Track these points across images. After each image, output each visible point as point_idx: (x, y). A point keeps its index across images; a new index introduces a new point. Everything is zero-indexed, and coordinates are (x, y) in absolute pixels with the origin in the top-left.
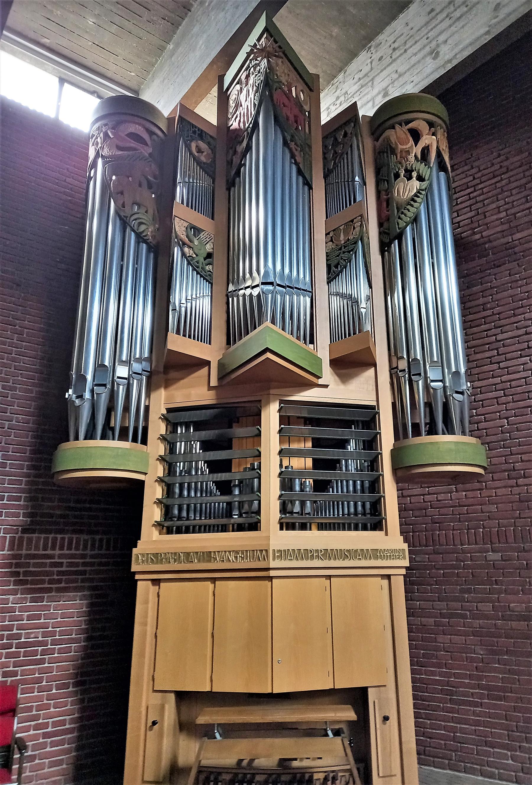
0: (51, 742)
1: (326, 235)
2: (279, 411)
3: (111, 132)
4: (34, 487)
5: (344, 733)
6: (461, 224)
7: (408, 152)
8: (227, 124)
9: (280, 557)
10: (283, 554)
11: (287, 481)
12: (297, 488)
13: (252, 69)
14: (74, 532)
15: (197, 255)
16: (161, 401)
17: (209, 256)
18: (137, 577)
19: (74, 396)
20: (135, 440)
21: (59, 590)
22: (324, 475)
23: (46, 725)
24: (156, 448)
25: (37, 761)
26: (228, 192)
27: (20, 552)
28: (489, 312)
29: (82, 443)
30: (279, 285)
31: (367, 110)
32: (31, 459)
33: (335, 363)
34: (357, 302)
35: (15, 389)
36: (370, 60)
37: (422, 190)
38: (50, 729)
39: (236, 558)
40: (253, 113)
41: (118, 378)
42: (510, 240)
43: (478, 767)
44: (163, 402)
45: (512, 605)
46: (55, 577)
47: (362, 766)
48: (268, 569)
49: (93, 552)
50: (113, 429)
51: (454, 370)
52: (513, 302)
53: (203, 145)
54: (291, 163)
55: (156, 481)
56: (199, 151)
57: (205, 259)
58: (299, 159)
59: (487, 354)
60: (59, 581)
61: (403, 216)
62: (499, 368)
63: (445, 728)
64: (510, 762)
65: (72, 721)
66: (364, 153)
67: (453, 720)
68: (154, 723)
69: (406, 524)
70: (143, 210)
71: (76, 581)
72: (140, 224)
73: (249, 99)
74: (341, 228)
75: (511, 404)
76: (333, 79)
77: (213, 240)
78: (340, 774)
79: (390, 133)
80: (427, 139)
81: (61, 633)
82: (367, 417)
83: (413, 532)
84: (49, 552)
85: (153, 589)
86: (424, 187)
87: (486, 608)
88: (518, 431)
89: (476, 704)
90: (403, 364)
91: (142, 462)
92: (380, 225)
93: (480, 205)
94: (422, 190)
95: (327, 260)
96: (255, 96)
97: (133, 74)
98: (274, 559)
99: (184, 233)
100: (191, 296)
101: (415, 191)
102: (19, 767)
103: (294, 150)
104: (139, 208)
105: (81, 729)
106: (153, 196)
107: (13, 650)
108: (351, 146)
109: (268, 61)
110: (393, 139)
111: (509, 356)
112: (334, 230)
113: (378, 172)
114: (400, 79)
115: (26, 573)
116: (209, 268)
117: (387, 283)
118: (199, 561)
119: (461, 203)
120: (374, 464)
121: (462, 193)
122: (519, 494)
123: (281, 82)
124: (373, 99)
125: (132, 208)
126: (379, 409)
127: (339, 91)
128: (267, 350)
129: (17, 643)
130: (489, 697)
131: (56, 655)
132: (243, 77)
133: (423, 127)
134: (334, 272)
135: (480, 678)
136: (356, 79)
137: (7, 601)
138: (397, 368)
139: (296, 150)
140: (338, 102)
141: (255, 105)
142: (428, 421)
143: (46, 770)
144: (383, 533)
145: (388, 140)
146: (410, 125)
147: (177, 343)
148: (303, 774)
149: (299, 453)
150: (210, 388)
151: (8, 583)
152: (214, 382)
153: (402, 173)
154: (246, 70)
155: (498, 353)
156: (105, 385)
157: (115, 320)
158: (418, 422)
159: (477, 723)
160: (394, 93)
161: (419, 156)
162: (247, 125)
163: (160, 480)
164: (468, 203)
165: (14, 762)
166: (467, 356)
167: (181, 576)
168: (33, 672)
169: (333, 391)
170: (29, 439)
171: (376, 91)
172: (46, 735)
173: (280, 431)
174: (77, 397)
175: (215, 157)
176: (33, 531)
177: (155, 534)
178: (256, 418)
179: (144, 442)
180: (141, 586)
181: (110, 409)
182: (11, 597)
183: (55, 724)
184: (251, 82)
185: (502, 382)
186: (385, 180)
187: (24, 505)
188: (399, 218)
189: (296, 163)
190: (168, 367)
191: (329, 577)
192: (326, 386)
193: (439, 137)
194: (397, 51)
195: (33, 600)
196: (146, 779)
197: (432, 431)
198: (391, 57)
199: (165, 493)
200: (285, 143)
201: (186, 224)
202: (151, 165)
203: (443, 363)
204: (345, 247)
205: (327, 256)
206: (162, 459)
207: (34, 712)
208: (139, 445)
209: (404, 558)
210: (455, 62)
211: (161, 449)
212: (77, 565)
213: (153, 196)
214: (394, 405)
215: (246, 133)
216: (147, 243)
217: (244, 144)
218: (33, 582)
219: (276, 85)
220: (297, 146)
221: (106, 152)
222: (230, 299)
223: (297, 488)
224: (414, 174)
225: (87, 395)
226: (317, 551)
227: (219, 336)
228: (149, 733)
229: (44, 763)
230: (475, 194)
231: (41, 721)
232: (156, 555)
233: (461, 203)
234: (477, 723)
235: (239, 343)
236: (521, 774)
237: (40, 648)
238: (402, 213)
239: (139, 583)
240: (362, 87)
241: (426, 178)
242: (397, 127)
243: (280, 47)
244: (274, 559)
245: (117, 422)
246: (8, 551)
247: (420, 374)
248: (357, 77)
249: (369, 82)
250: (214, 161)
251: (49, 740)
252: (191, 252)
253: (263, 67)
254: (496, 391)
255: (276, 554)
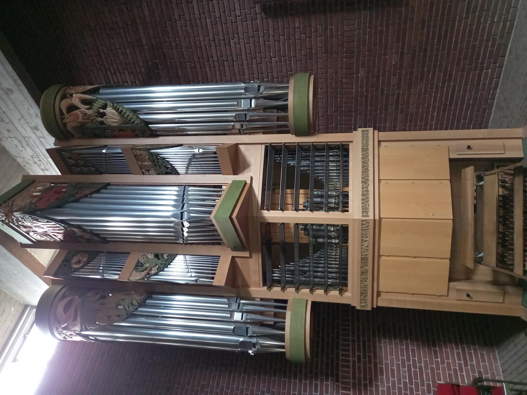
0: (470, 361)
1: (144, 174)
2: (268, 210)
3: (63, 325)
4: (309, 375)
5: (480, 175)
6: (133, 80)
7: (85, 114)
8: (59, 242)
9: (367, 212)
10: (365, 210)
11: (314, 207)
12: (319, 200)
13: (20, 223)
14: (338, 348)
15: (157, 265)
16: (259, 291)
17: (157, 256)
18: (375, 306)
19: (253, 349)
20: (285, 308)
21: (375, 358)
22: (311, 183)
23: (460, 364)
24: (290, 294)
25: (482, 370)
26: (110, 243)
27: (351, 383)
28: (198, 65)
29: (287, 343)
30: (182, 208)
31: (50, 142)
32: (290, 377)
33: (236, 172)
34: (194, 155)
35: (242, 389)
36: (9, 139)
37: (113, 105)
38: (462, 362)
39: (366, 241)
40: (53, 223)
41: (242, 319)
42: (147, 47)
43: (492, 91)
44: (259, 289)
45: (393, 63)
46: (367, 360)
47: (496, 164)
48: (374, 220)
49: (351, 335)
50: (275, 323)
51: (243, 91)
52: (191, 48)
53: (75, 259)
54: (91, 197)
55: (312, 294)
56: (79, 262)
57: (159, 259)
58: (88, 192)
59: (227, 68)
60: (370, 357)
61: (132, 121)
62: (237, 61)
63: (467, 110)
64: (490, 71)
65: (457, 348)
66: (83, 146)
67: (462, 105)
68: (468, 296)
69: (337, 129)
70: (122, 302)
71: (369, 347)
72: (132, 304)
73: (42, 226)
74: (140, 163)
75: (262, 55)
76: (21, 165)
77: (146, 254)
78: (500, 178)
79: (70, 126)
80: (76, 100)
81: (402, 355)
82: (272, 152)
83: (342, 125)
84: (351, 364)
85: (383, 296)
86: (112, 105)
87: (394, 80)
88: (280, 51)
89: (453, 91)
90: (238, 125)
91: (299, 306)
92: (137, 136)
93: (120, 67)
94: (113, 105)
95: (162, 174)
96: (40, 222)
97: (13, 309)
98: (368, 216)
99: (141, 273)
100: (179, 270)
101: (114, 111)
102: (492, 382)
103: (82, 195)
104: (120, 305)
105: (462, 343)
106: (110, 295)
107: (413, 386)
108: (79, 154)
109: (16, 211)
110: (74, 124)
111: (229, 54)
112: (141, 169)
113: (98, 136)
114: (26, 118)
115: (365, 379)
116: (165, 256)
117: (180, 133)
118: (367, 266)
119: (118, 79)
120: (303, 148)
121: (111, 78)
122: (322, 53)
123: (30, 202)
124: (39, 138)
125: (120, 309)
126: (268, 143)
127: (30, 162)
128: (230, 218)
129: (410, 385)
130: (450, 81)
131: (416, 359)
132: (25, 230)
133: (65, 104)
134: (173, 171)
135: (437, 86)
136: (23, 150)
137: (383, 391)
138: (239, 130)
139: (81, 193)
140: (38, 162)
141: (47, 222)
142: (276, 111)
143: (487, 364)
144: (351, 144)
145: (75, 128)
146: (65, 112)
147: (220, 279)
148: (500, 201)
149: (284, 198)
150: (251, 257)
151: (371, 391)
152: (247, 254)
153: (100, 119)
154: (19, 227)
155: (226, 61)
156: (247, 328)
157: (181, 320)
158: (276, 117)
159: (465, 91)
160: (39, 122)
161: (88, 107)
162: (62, 228)
163: (312, 291)
164: (118, 74)
165: (489, 385)
166: (227, 82)
167: (375, 278)
168: (427, 374)
169: (255, 174)
170: (277, 379)
171: (33, 135)
172: (466, 365)
173: (282, 210)
174: (255, 347)
175: (84, 252)
176: (338, 375)
177: (347, 294)
178: (269, 226)
179: (286, 301)
180: (381, 303)
181: (262, 324)
182: (380, 389)
183: (459, 359)
184: (29, 224)
185: (247, 60)
186: (105, 131)
187: (321, 381)
188: (133, 123)
189: (92, 193)
190: (235, 286)
191: (379, 180)
192: (252, 178)
193: (73, 92)
194: (3, 119)
195: (382, 374)
196: (501, 301)
197: (284, 108)
198: (8, 123)
199: (291, 286)
200: (77, 201)
201: (134, 272)
202: (88, 297)
203: (238, 98)
204: (154, 162)
205: (159, 174)
206: (297, 290)
207: (452, 372)
208: (289, 305)
209: (368, 131)
210: (16, 77)
211: (291, 290)
212: (359, 345)
213: (110, 295)
214: (264, 133)
215: (68, 229)
216: (146, 300)
217: (76, 230)
218: (371, 374)
219: (33, 206)
220: (78, 192)
221: (77, 328)
222: (189, 242)
223: (319, 200)
224: (102, 111)
225: (254, 340)
226: (363, 188)
227: (215, 250)
228: (474, 299)
229: (483, 365)
230: (112, 69)
231: (457, 368)
232: (362, 294)
233: (118, 79)
234: (465, 91)
235: (222, 236)
236: (497, 64)
237: (412, 369)
238: (130, 120)
239: (379, 305)
240: (29, 145)
241: (104, 102)
242: (64, 121)
243: (4, 202)
244: (368, 216)
245: (271, 320)
246: (350, 391)
247: (246, 114)
248: (20, 148)
249: (25, 140)
250: (87, 252)
251: (411, 358)
252: (154, 268)
253: (19, 216)
254: (252, 64)
255: (365, 214)
